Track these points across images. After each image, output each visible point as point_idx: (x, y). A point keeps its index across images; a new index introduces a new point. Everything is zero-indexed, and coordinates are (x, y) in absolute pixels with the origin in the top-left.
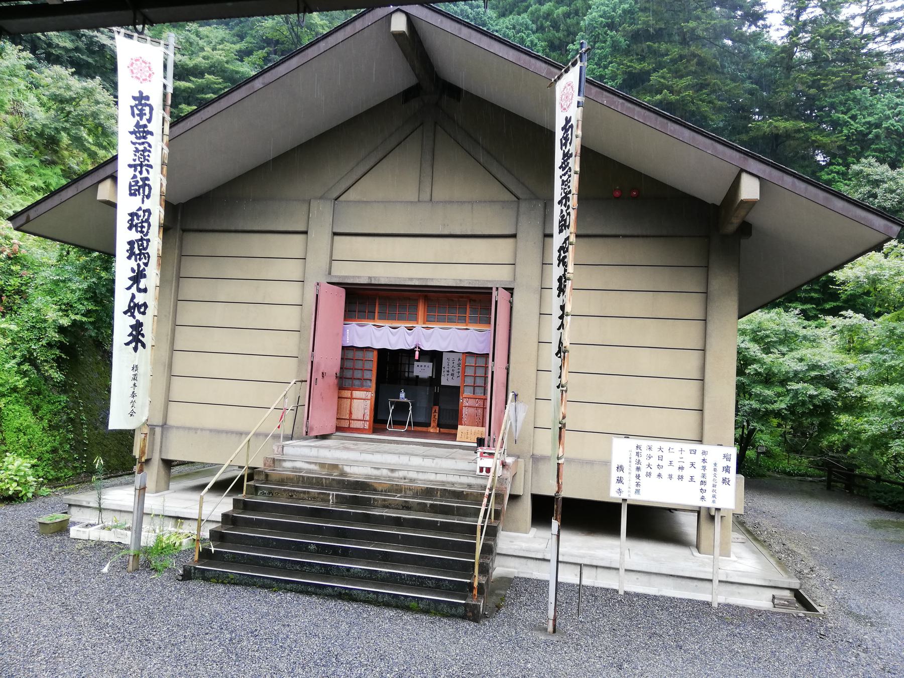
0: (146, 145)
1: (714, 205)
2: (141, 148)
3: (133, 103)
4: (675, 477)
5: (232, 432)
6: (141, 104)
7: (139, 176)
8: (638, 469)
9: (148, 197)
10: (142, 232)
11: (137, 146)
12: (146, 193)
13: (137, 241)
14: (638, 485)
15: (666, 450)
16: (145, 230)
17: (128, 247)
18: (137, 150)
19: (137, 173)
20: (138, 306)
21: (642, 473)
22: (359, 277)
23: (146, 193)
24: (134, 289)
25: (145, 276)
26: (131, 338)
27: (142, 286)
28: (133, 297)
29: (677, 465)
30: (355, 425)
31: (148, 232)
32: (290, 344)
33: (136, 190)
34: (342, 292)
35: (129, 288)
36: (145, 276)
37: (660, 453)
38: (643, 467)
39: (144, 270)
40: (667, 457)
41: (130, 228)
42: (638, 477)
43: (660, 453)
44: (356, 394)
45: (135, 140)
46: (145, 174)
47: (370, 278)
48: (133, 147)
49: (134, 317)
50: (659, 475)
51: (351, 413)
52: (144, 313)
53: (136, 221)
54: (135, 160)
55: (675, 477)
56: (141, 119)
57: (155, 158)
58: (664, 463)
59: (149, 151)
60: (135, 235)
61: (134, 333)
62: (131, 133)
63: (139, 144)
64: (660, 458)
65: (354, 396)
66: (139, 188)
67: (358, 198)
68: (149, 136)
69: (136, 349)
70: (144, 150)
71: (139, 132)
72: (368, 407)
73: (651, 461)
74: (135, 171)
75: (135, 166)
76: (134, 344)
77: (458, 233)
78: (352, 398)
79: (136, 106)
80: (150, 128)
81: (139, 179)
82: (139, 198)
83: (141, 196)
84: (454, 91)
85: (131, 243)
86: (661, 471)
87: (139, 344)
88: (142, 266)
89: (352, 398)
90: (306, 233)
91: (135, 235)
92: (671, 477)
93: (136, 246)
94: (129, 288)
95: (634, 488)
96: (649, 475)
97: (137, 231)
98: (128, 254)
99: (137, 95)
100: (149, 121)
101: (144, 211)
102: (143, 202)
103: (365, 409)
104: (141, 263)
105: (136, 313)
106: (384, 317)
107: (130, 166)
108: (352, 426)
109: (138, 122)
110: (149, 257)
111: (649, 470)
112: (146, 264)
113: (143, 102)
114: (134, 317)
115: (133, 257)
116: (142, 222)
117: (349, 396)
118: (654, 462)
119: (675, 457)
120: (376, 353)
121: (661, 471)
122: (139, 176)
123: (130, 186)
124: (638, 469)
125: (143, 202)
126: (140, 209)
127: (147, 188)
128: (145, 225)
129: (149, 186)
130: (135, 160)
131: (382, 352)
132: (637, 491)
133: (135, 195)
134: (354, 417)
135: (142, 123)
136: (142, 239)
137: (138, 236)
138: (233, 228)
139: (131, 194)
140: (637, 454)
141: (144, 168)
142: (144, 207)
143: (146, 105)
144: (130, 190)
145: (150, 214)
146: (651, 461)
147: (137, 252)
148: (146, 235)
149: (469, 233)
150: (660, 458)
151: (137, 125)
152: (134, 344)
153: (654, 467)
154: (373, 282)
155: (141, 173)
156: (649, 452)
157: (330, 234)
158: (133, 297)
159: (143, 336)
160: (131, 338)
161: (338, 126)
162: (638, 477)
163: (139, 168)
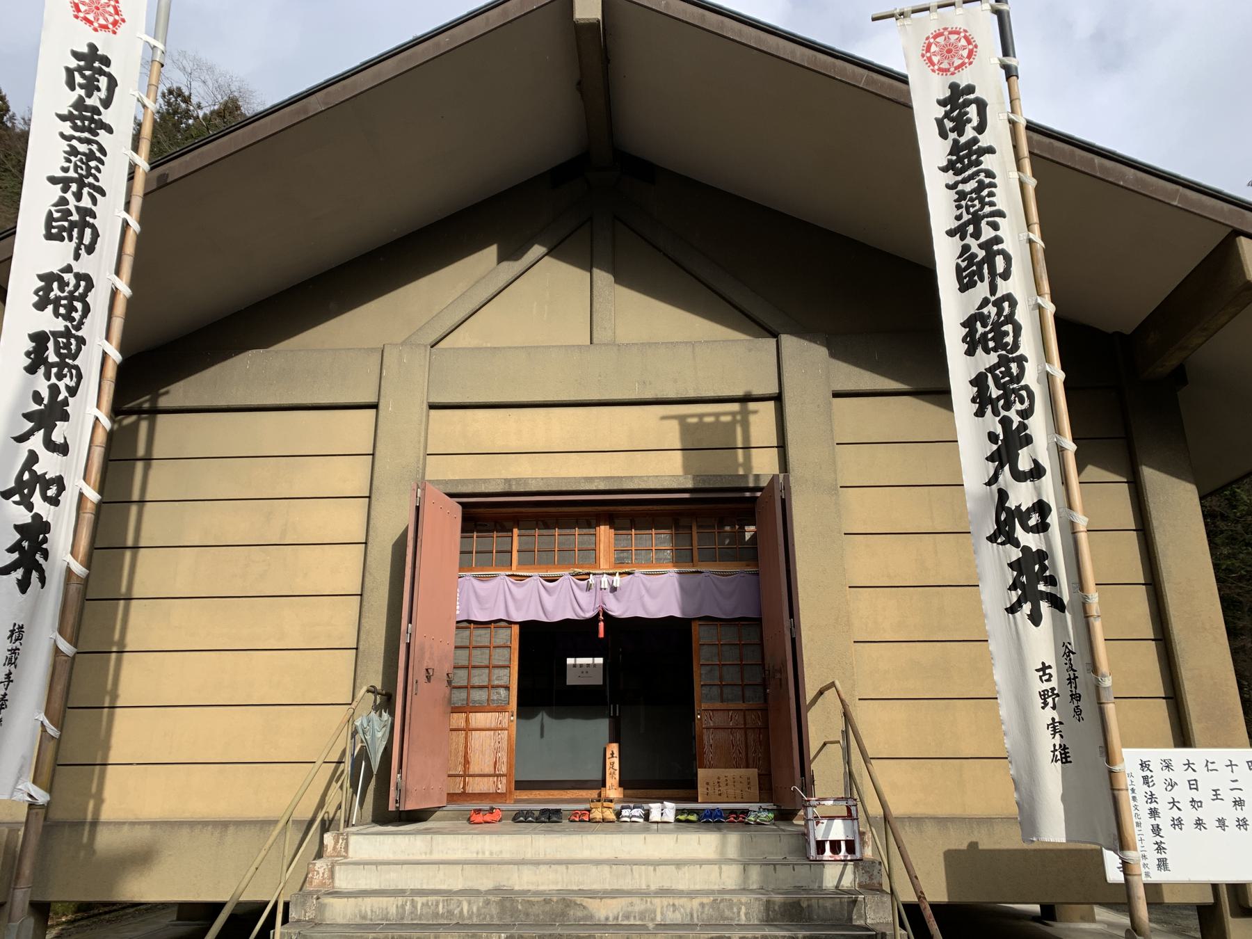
0: (94, 147)
1: (1119, 335)
2: (83, 148)
3: (73, 63)
4: (1231, 823)
5: (205, 824)
6: (91, 68)
7: (72, 202)
8: (1154, 813)
9: (90, 249)
10: (67, 317)
11: (74, 142)
12: (87, 240)
13: (56, 334)
14: (1160, 848)
15: (1199, 766)
16: (76, 316)
17: (30, 345)
18: (74, 151)
19: (69, 196)
20: (45, 483)
21: (1164, 822)
22: (485, 481)
23: (87, 240)
24: (36, 443)
25: (65, 417)
26: (16, 555)
27: (57, 437)
28: (33, 458)
29: (1229, 797)
30: (477, 786)
31: (81, 323)
32: (339, 621)
33: (62, 229)
34: (458, 511)
35: (21, 439)
36: (65, 417)
37: (1191, 775)
38: (1163, 807)
39: (65, 402)
40: (1207, 782)
41: (40, 306)
42: (1156, 830)
43: (1191, 775)
44: (479, 719)
45: (69, 131)
46: (86, 202)
47: (507, 481)
48: (64, 146)
49: (30, 507)
50: (1199, 823)
51: (467, 762)
52: (54, 501)
53: (56, 292)
54: (66, 170)
55: (1231, 823)
56: (89, 95)
57: (113, 176)
58: (1204, 794)
59: (102, 163)
60: (49, 322)
61: (25, 544)
62: (63, 118)
63: (81, 140)
64: (1194, 785)
65: (473, 724)
66: (71, 225)
67: (474, 343)
68: (102, 132)
69: (23, 585)
70: (90, 156)
71: (83, 118)
72: (505, 744)
73: (1176, 793)
74: (65, 190)
75: (65, 183)
76: (19, 574)
77: (672, 395)
78: (468, 729)
79: (80, 70)
80: (107, 116)
81: (71, 207)
82: (68, 247)
83: (73, 244)
84: (644, 171)
85: (40, 339)
86: (1200, 813)
87: (35, 575)
88: (64, 394)
89: (468, 729)
90: (375, 406)
91: (49, 322)
92: (1222, 823)
93: (51, 345)
94: (21, 439)
95: (1153, 857)
96: (1177, 823)
97: (57, 314)
98: (28, 361)
99: (84, 49)
100: (107, 103)
101: (79, 277)
102: (77, 257)
103: (497, 751)
104: (61, 385)
105: (37, 498)
106: (530, 557)
107: (53, 180)
108: (469, 790)
109: (81, 99)
110: (80, 377)
111: (1176, 814)
112: (73, 391)
113: (97, 64)
114: (30, 507)
115: (42, 370)
116: (71, 297)
117: (463, 725)
118: (1183, 794)
119: (1222, 779)
120: (516, 629)
121: (1200, 813)
122: (72, 202)
123: (50, 218)
124: (1154, 813)
125: (77, 257)
126: (68, 269)
127: (88, 231)
128: (78, 305)
129: (93, 227)
130: (66, 170)
131: (530, 630)
132: (1162, 864)
133: (62, 239)
134: (474, 769)
135: (89, 102)
136: (67, 334)
137: (60, 325)
138: (222, 403)
139: (49, 236)
140: (1145, 779)
141: (86, 190)
142: (78, 267)
143: (102, 73)
144: (49, 226)
145: (90, 286)
146: (1176, 793)
147: (52, 358)
148: (78, 328)
149: (692, 394)
150: (1194, 785)
151: (79, 104)
152: (19, 574)
153: (1185, 804)
154: (514, 489)
155: (78, 196)
156: (1167, 774)
157: (425, 406)
158: (33, 458)
159: (46, 554)
160: (16, 555)
161: (431, 225)
162: (1156, 830)
163: (74, 187)
